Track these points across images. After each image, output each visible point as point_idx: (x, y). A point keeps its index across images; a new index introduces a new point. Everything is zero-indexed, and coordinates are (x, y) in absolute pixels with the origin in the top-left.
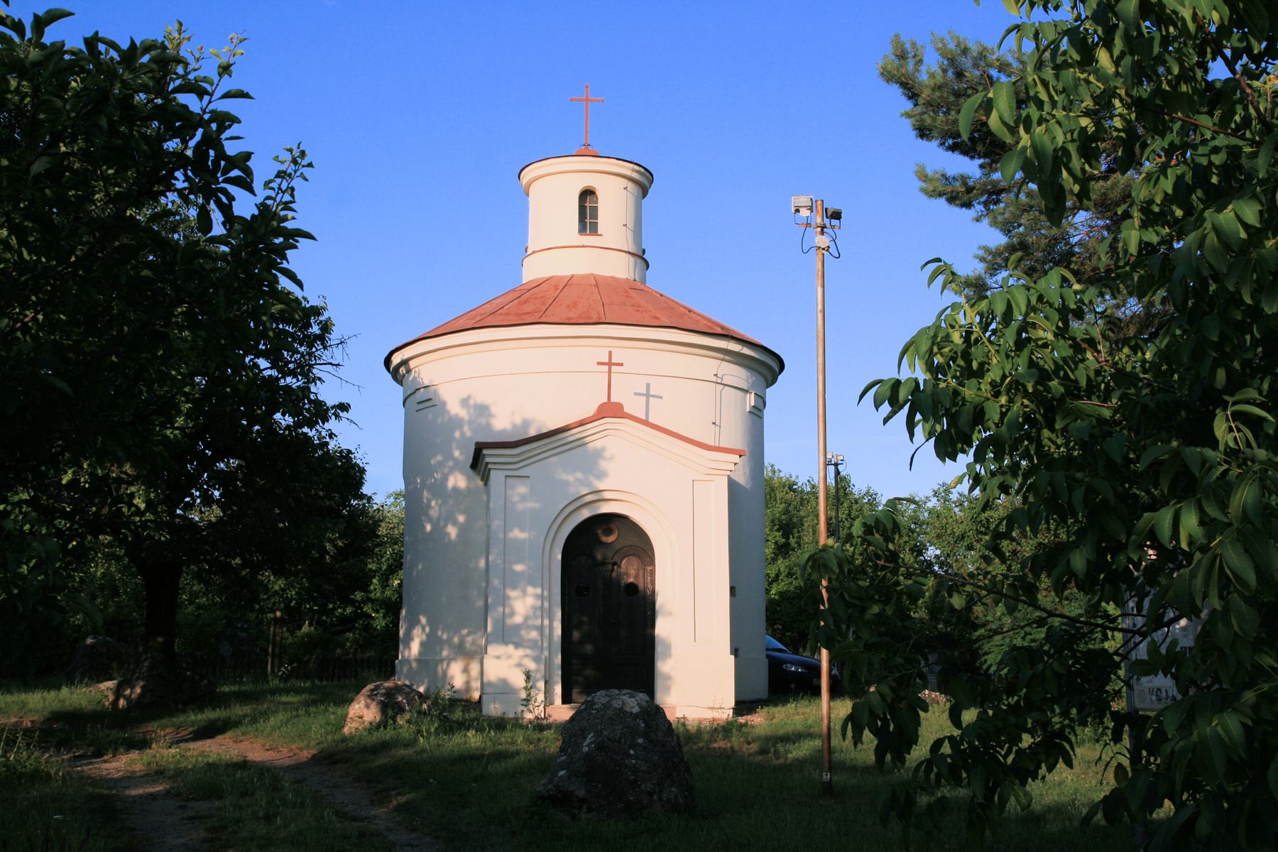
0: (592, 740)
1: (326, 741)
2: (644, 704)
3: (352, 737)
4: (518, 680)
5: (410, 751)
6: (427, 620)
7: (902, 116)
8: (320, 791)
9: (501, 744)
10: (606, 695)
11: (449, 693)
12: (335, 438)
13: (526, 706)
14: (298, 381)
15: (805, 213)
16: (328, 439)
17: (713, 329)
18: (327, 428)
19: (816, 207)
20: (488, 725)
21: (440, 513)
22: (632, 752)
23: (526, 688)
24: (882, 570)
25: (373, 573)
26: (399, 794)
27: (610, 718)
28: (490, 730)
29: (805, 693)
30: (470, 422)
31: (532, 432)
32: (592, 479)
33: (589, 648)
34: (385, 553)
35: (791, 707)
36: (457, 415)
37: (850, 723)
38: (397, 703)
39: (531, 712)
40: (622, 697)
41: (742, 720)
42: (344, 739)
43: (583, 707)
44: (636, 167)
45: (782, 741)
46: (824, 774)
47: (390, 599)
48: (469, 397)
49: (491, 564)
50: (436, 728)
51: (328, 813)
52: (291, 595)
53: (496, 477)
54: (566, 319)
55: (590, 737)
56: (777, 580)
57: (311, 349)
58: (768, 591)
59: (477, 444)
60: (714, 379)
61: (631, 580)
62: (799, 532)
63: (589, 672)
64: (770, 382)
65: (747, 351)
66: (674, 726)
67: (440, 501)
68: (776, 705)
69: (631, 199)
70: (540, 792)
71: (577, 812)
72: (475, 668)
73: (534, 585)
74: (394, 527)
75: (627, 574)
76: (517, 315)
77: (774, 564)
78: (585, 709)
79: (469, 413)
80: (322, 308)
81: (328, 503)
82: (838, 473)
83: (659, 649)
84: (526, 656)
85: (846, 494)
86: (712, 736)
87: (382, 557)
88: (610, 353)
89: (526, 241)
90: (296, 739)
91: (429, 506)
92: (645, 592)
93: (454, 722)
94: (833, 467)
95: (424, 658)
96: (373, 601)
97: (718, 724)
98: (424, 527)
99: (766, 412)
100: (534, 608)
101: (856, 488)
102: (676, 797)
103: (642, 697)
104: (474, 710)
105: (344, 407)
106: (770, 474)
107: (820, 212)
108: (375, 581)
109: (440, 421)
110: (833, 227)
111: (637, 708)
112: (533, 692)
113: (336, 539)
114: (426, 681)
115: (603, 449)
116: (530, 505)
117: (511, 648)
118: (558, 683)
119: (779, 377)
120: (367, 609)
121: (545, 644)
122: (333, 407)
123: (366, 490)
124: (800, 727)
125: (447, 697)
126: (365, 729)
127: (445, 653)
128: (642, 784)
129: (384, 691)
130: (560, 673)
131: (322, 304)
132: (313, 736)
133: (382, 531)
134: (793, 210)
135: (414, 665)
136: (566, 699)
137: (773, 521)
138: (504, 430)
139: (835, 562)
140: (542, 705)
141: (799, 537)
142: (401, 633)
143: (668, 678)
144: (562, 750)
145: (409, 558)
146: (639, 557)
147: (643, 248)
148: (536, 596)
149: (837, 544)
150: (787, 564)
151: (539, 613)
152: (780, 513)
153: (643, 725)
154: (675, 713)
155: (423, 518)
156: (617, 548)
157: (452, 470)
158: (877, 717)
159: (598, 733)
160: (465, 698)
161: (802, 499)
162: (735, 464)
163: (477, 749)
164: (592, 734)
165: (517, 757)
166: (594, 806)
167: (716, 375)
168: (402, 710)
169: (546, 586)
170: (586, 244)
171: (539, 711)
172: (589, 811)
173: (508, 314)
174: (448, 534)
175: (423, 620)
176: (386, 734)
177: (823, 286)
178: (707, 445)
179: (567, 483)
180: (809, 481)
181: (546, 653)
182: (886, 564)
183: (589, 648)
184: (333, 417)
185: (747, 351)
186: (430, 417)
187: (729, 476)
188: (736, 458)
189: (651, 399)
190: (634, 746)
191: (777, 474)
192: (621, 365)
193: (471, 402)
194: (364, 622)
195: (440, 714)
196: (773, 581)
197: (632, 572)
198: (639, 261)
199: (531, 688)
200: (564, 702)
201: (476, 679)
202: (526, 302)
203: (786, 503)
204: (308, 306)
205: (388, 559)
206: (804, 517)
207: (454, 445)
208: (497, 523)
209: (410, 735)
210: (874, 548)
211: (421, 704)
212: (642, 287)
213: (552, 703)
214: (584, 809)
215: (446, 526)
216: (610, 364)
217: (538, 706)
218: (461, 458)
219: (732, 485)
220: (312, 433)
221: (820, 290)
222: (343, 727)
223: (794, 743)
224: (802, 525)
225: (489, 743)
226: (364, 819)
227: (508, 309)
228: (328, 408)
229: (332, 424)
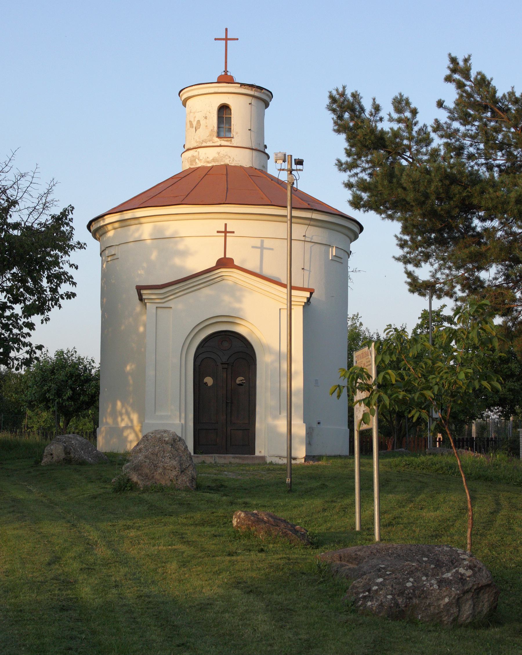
7: (470, 56)
60: (303, 238)
88: (226, 225)
119: (360, 235)
167: (304, 236)
192: (233, 232)
216: (226, 232)
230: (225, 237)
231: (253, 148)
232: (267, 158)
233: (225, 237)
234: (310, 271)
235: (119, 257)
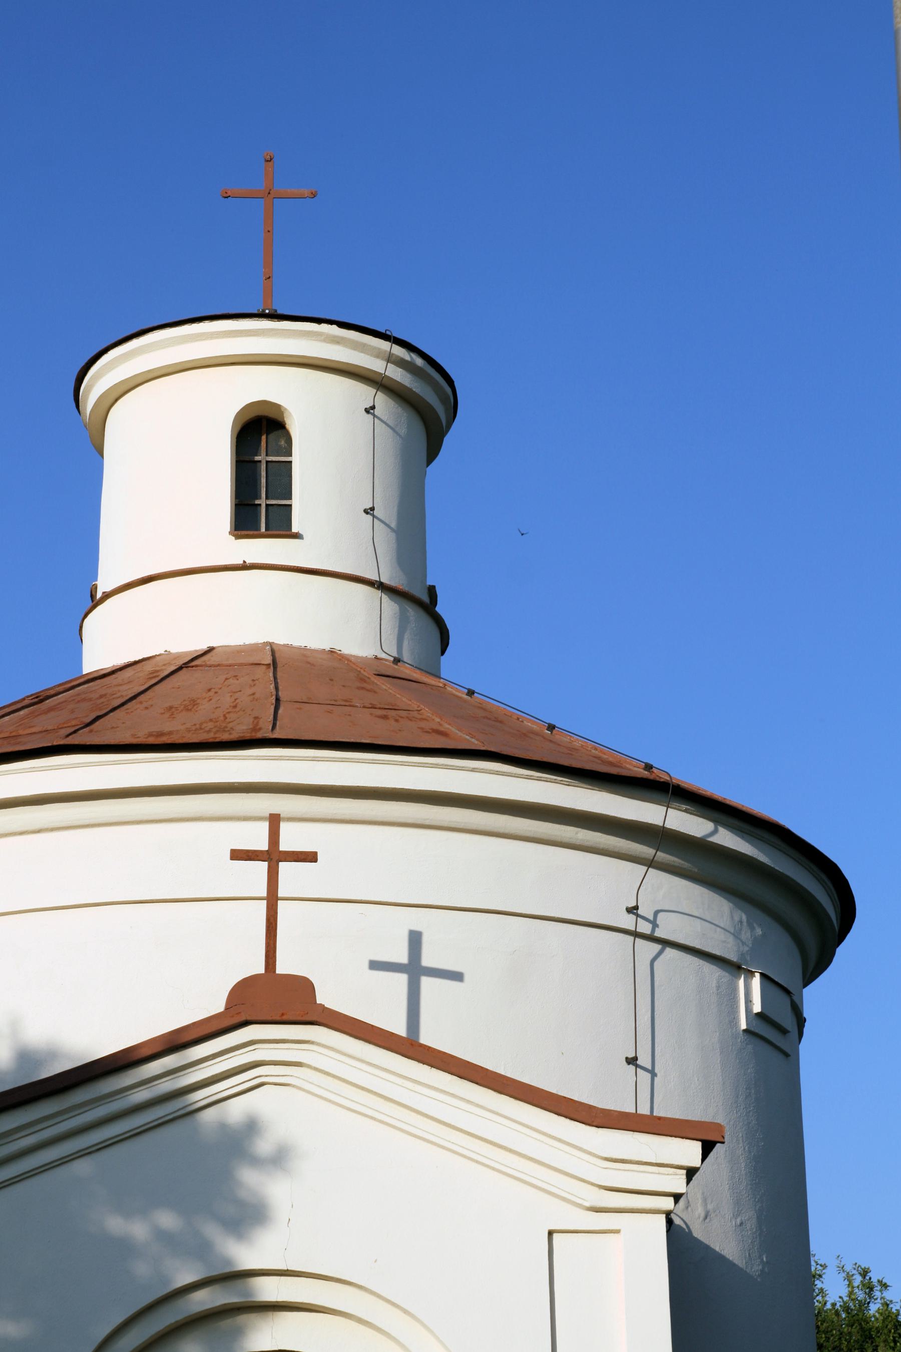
32: (212, 1231)
44: (398, 351)
60: (628, 922)
65: (727, 838)
89: (94, 575)
99: (806, 1049)
106: (861, 1295)
167: (633, 910)
170: (249, 561)
185: (727, 838)
187: (668, 1214)
189: (427, 983)
191: (877, 1294)
198: (413, 612)
231: (384, 580)
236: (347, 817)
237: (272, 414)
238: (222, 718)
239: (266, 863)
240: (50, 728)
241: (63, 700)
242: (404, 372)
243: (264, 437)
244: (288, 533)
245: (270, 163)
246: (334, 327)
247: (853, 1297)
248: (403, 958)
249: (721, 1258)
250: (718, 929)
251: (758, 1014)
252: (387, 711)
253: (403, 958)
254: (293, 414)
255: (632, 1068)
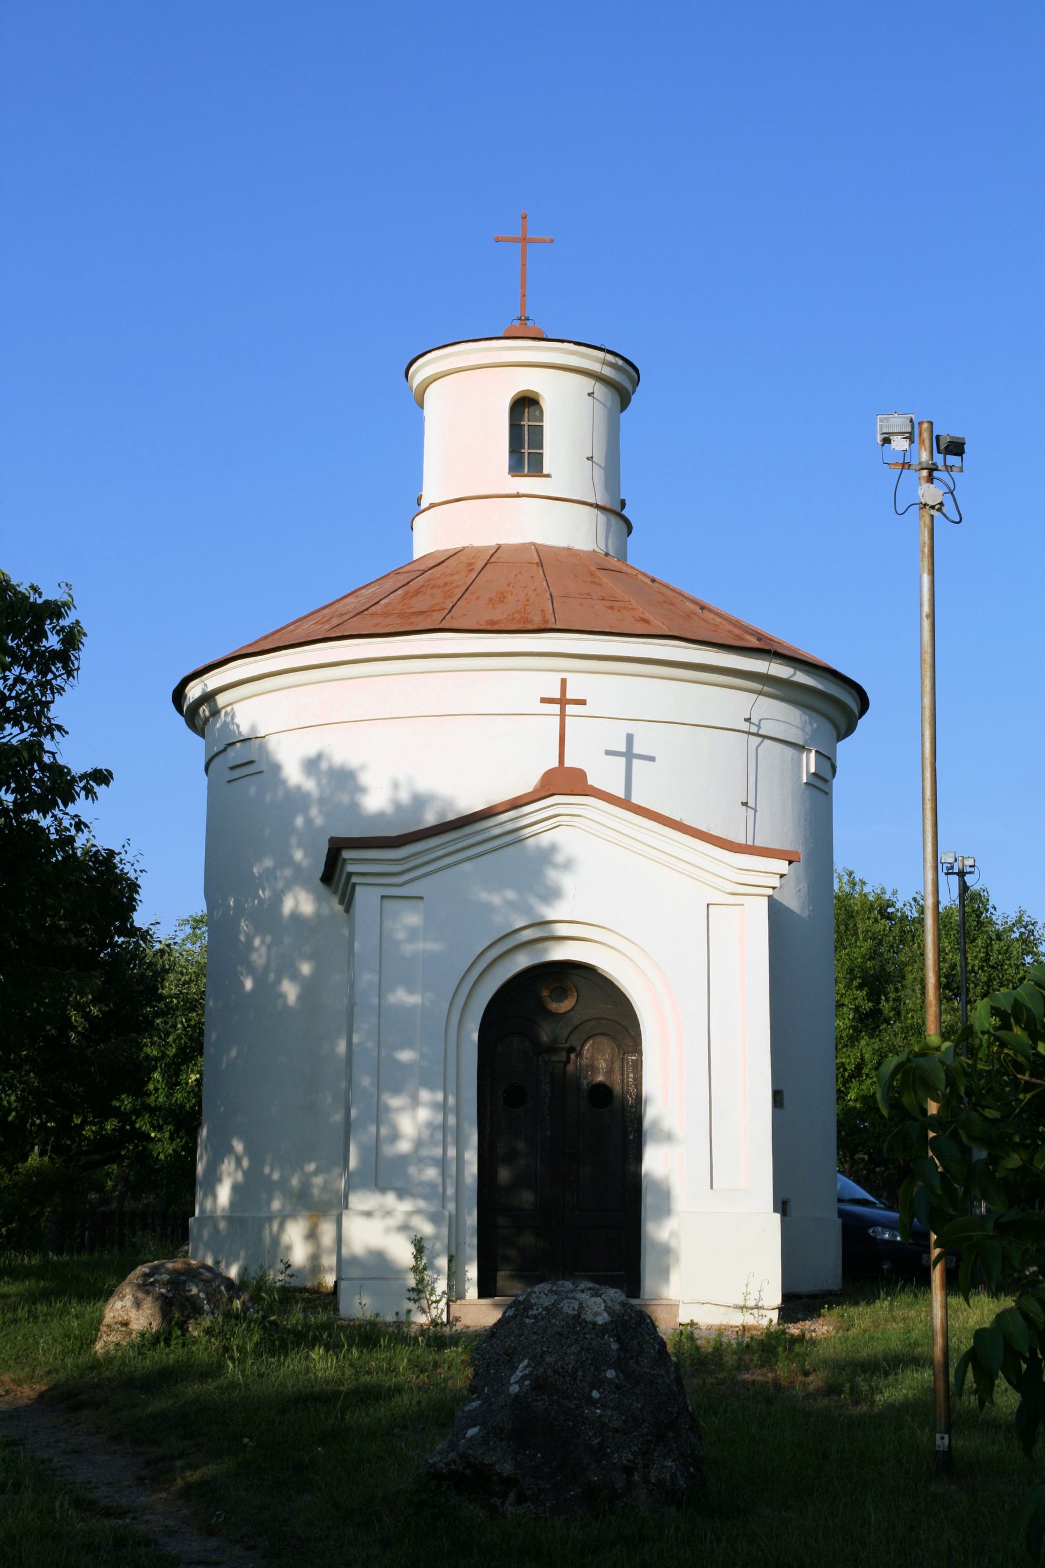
0: (527, 1372)
1: (64, 1368)
2: (617, 1308)
3: (109, 1359)
4: (403, 1253)
5: (211, 1386)
6: (245, 1149)
8: (51, 1460)
9: (369, 1373)
10: (551, 1291)
11: (281, 1277)
12: (86, 830)
13: (415, 1301)
14: (22, 731)
15: (900, 444)
16: (73, 832)
17: (742, 639)
18: (72, 813)
19: (920, 434)
20: (347, 1338)
21: (268, 962)
22: (595, 1394)
23: (415, 1269)
24: (1026, 1091)
25: (150, 1065)
26: (189, 1466)
27: (558, 1333)
28: (350, 1346)
29: (908, 1281)
30: (322, 801)
31: (430, 819)
32: (533, 901)
33: (527, 1197)
34: (174, 1026)
35: (882, 1306)
36: (299, 788)
37: (970, 1365)
38: (187, 1299)
39: (424, 1312)
40: (579, 1295)
41: (794, 1330)
42: (96, 1365)
43: (510, 1313)
44: (610, 358)
45: (864, 1372)
46: (938, 1436)
47: (182, 1106)
48: (319, 757)
49: (355, 1049)
50: (257, 1344)
51: (62, 1505)
52: (9, 1102)
53: (365, 897)
54: (488, 623)
55: (523, 1367)
56: (860, 1075)
57: (45, 675)
58: (841, 1095)
59: (333, 840)
60: (745, 726)
61: (600, 1078)
62: (897, 990)
63: (527, 1240)
64: (843, 731)
65: (802, 678)
66: (670, 1348)
67: (268, 939)
68: (856, 1303)
69: (601, 413)
70: (434, 1465)
71: (498, 1502)
72: (327, 1232)
73: (432, 1088)
74: (191, 981)
75: (593, 1068)
76: (402, 615)
77: (853, 1046)
78: (514, 1317)
79: (319, 784)
80: (65, 604)
81: (74, 941)
82: (964, 888)
83: (648, 1200)
84: (418, 1212)
85: (980, 924)
86: (740, 1359)
87: (168, 1034)
88: (564, 682)
89: (421, 489)
90: (11, 1362)
91: (249, 946)
92: (623, 1099)
93: (289, 1331)
94: (956, 877)
95: (238, 1214)
96: (152, 1110)
97: (752, 1338)
98: (242, 985)
100: (430, 1125)
101: (998, 913)
102: (673, 1476)
103: (614, 1295)
104: (325, 1308)
105: (102, 777)
106: (847, 889)
107: (927, 442)
108: (156, 1075)
109: (268, 798)
110: (949, 469)
111: (605, 1315)
112: (428, 1275)
113: (87, 1004)
114: (242, 1254)
115: (553, 848)
116: (421, 946)
117: (390, 1199)
118: (471, 1259)
120: (142, 1124)
121: (451, 1191)
122: (82, 777)
123: (140, 919)
124: (895, 1345)
125: (279, 1284)
126: (132, 1345)
127: (276, 1205)
128: (613, 1453)
129: (165, 1277)
130: (475, 1241)
131: (66, 598)
132: (41, 1358)
133: (169, 987)
134: (879, 438)
135: (222, 1225)
136: (484, 1291)
137: (851, 971)
138: (381, 816)
139: (942, 1075)
140: (444, 1300)
141: (898, 1000)
142: (200, 1168)
143: (666, 1251)
144: (473, 1389)
145: (214, 1036)
146: (614, 1039)
147: (622, 497)
148: (435, 1106)
149: (947, 1044)
150: (876, 1047)
151: (439, 1136)
152: (863, 957)
153: (615, 1346)
154: (676, 1316)
155: (239, 968)
156: (577, 1021)
157: (289, 885)
158: (1020, 1355)
159: (537, 1360)
160: (309, 1285)
161: (902, 931)
162: (782, 876)
163: (327, 1382)
164: (526, 1362)
165: (397, 1399)
166: (529, 1493)
167: (748, 720)
168: (197, 1310)
169: (452, 1087)
170: (522, 492)
171: (439, 1311)
172: (521, 1500)
173: (385, 614)
174: (283, 996)
175: (239, 1147)
176: (168, 1354)
177: (932, 573)
178: (732, 842)
179: (489, 908)
180: (915, 899)
181: (451, 1206)
182: (1034, 1080)
183: (527, 1197)
184: (83, 793)
185: (802, 678)
186: (253, 791)
188: (782, 866)
189: (636, 762)
190: (599, 1383)
191: (858, 888)
192: (583, 702)
193: (324, 766)
194: (136, 1146)
195: (264, 1318)
196: (851, 1076)
197: (602, 1064)
198: (614, 520)
199: (425, 1269)
200: (481, 1295)
201: (331, 1252)
202: (417, 593)
203: (873, 939)
204: (40, 601)
205: (179, 1037)
206: (906, 964)
207: (294, 840)
208: (367, 978)
209: (210, 1356)
210: (1011, 1052)
211: (230, 1300)
212: (619, 566)
213: (461, 1296)
214: (512, 1497)
215: (278, 981)
216: (563, 701)
217: (437, 1302)
218: (305, 863)
219: (776, 911)
220: (45, 822)
221: (926, 579)
222: (94, 1341)
223: (887, 1375)
224: (903, 977)
225: (348, 1372)
226: (127, 1512)
227: (389, 604)
228: (73, 778)
229: (81, 807)
230: (563, 715)
231: (599, 503)
232: (626, 534)
233: (563, 715)
234: (755, 810)
235: (264, 768)
236: (595, 670)
237: (531, 396)
238: (523, 610)
239: (559, 705)
240: (424, 610)
241: (420, 584)
242: (611, 369)
243: (526, 410)
244: (539, 474)
245: (525, 220)
246: (572, 344)
247: (842, 890)
248: (623, 749)
249: (787, 909)
250: (794, 727)
251: (813, 774)
252: (612, 602)
253: (623, 749)
254: (545, 397)
255: (745, 807)
